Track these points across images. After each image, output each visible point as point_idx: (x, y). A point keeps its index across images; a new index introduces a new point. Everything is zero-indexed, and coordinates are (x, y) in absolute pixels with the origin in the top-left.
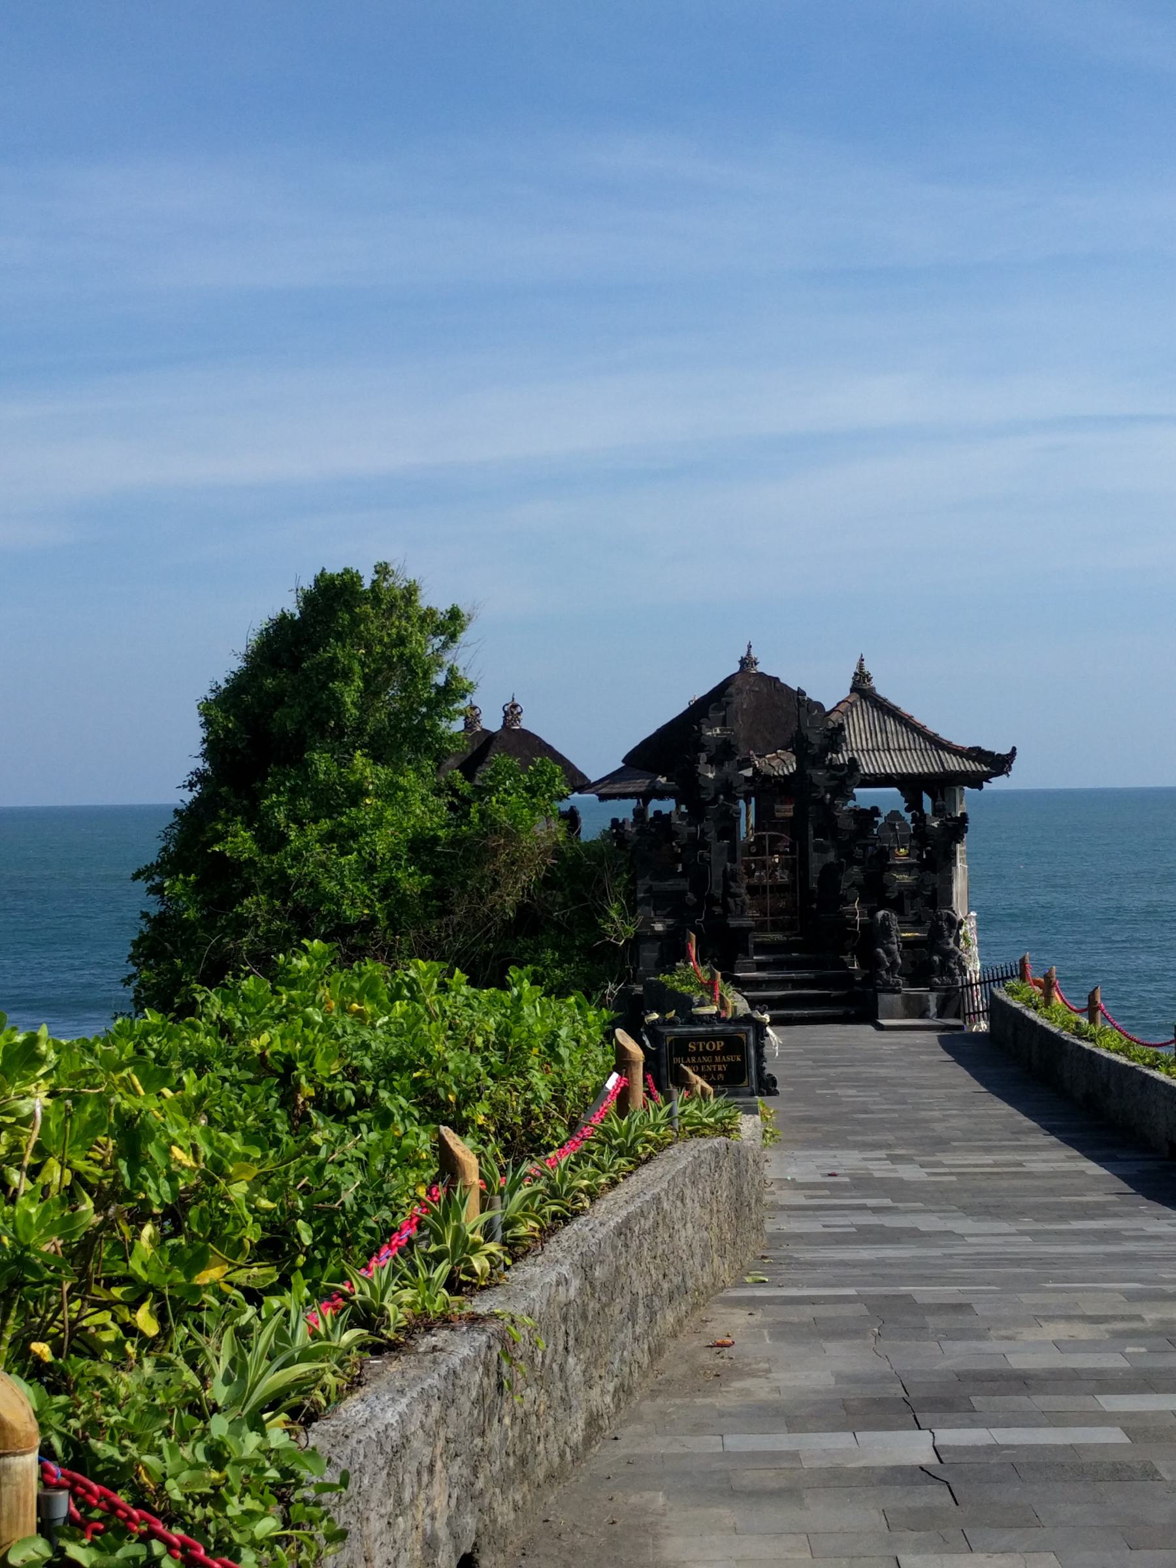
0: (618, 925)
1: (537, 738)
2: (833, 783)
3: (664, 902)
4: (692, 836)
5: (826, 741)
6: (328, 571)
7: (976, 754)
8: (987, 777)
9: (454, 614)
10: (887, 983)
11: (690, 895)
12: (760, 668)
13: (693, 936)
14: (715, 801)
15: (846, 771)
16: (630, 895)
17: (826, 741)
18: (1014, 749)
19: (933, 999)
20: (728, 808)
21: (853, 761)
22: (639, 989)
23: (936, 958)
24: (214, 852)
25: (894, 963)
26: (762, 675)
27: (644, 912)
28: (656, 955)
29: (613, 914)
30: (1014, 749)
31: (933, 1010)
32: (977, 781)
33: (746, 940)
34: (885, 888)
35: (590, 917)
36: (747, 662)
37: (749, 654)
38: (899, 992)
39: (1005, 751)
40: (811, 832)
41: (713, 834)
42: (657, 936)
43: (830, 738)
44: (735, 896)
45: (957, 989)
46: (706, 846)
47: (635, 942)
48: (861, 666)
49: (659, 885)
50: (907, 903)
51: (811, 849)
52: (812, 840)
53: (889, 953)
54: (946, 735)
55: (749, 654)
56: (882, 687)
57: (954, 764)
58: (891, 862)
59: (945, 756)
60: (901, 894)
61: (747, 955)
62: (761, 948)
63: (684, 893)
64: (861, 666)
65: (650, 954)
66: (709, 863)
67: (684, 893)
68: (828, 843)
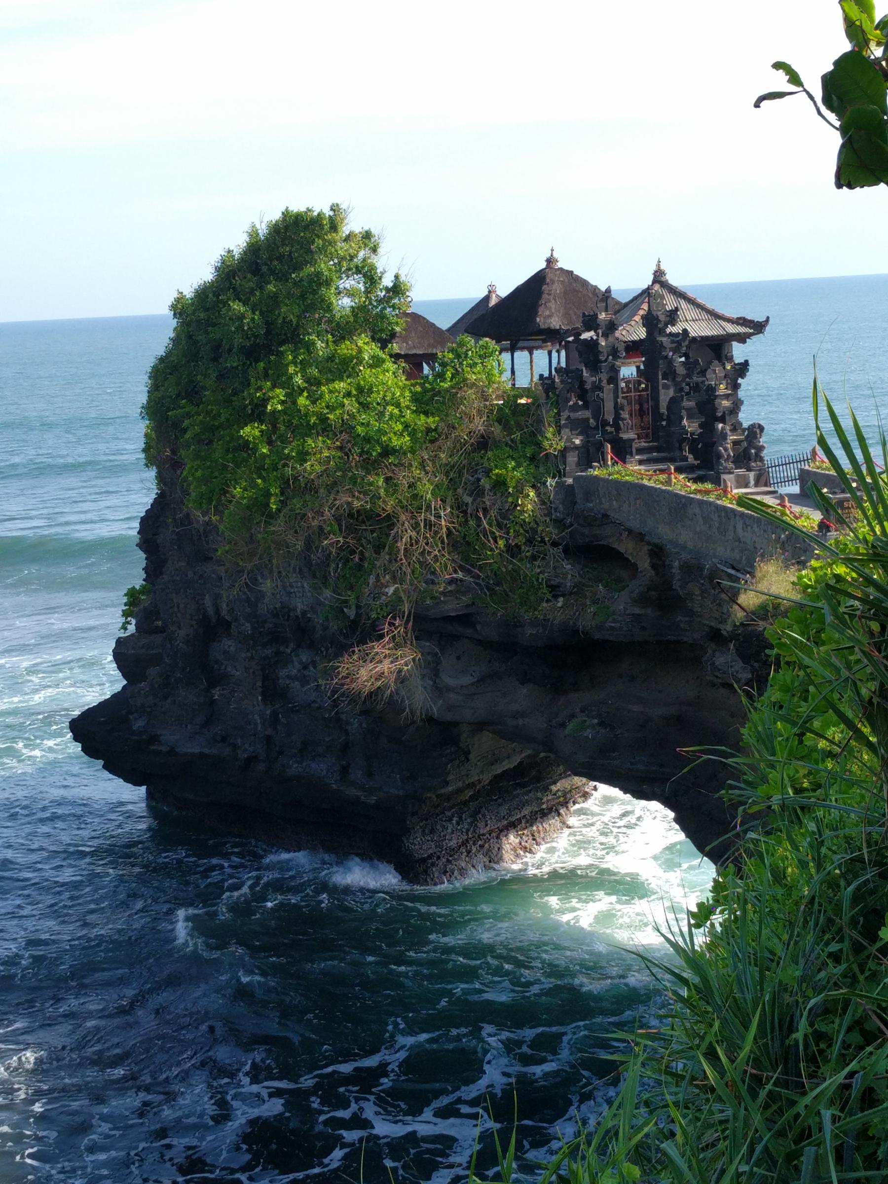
0: (553, 441)
1: (424, 318)
2: (674, 345)
3: (581, 427)
4: (594, 383)
5: (668, 319)
6: (290, 209)
7: (742, 321)
8: (749, 336)
9: (367, 235)
10: (726, 468)
11: (592, 421)
12: (560, 265)
13: (609, 446)
14: (606, 360)
15: (681, 337)
16: (557, 422)
17: (668, 319)
18: (768, 318)
19: (752, 475)
20: (613, 365)
21: (685, 331)
22: (570, 481)
23: (753, 451)
24: (682, 418)
25: (729, 455)
26: (561, 269)
27: (566, 432)
28: (576, 459)
29: (549, 435)
30: (768, 318)
31: (752, 482)
32: (742, 338)
33: (631, 446)
34: (715, 410)
35: (533, 438)
36: (550, 261)
37: (552, 255)
38: (733, 473)
39: (762, 319)
40: (660, 377)
41: (605, 381)
42: (576, 448)
43: (670, 316)
44: (623, 419)
45: (764, 470)
46: (600, 389)
47: (564, 452)
48: (658, 265)
49: (574, 415)
50: (727, 418)
51: (660, 388)
52: (662, 382)
53: (726, 449)
54: (720, 311)
55: (552, 255)
56: (673, 279)
57: (731, 329)
58: (717, 393)
59: (723, 323)
60: (724, 413)
61: (631, 455)
62: (640, 451)
63: (588, 419)
64: (658, 265)
65: (572, 458)
66: (603, 400)
67: (588, 419)
68: (669, 383)
